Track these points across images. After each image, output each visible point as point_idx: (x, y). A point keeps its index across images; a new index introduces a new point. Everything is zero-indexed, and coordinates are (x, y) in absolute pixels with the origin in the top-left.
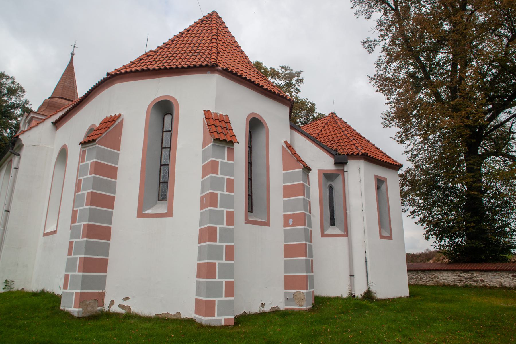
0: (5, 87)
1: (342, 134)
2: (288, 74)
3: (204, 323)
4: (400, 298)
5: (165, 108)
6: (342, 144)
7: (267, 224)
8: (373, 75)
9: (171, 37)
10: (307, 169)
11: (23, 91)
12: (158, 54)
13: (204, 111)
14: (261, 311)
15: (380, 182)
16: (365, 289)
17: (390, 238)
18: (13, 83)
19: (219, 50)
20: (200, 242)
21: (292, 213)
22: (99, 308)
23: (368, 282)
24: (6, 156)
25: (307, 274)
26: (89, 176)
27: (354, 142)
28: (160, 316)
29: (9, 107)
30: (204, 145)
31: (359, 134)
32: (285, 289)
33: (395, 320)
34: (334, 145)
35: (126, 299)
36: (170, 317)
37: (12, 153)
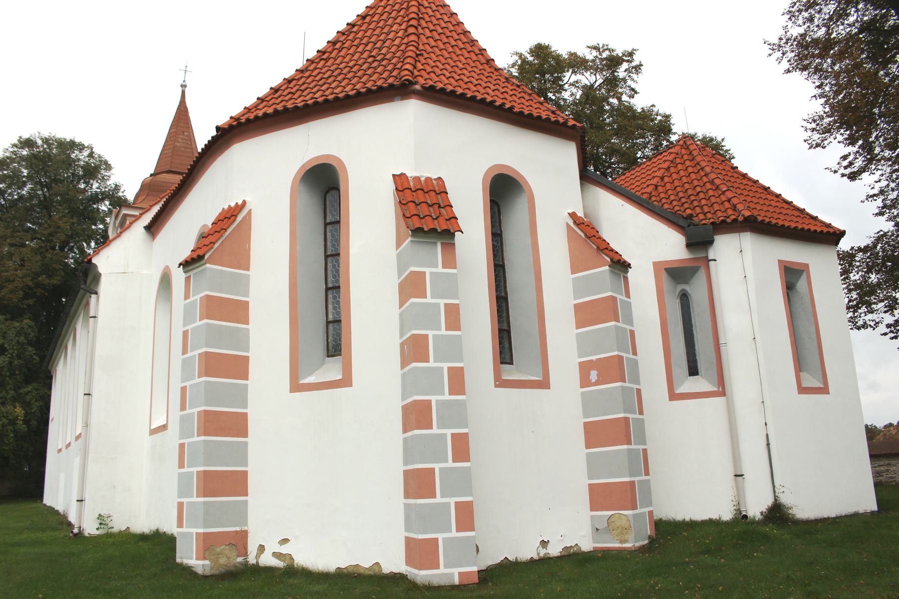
0: (78, 166)
1: (705, 179)
2: (605, 59)
3: (419, 581)
4: (856, 515)
5: (324, 182)
6: (704, 202)
7: (544, 384)
8: (778, 36)
9: (332, 36)
10: (620, 266)
11: (108, 167)
12: (307, 74)
13: (394, 176)
14: (542, 555)
15: (792, 276)
16: (769, 501)
17: (824, 390)
18: (91, 155)
19: (421, 47)
20: (405, 431)
21: (594, 358)
22: (240, 559)
23: (774, 487)
24: (79, 296)
25: (633, 479)
26: (199, 323)
27: (729, 194)
28: (345, 571)
29: (89, 200)
30: (398, 244)
31: (745, 176)
32: (592, 510)
33: (811, 563)
34: (686, 206)
35: (285, 541)
36: (362, 571)
37: (87, 291)
